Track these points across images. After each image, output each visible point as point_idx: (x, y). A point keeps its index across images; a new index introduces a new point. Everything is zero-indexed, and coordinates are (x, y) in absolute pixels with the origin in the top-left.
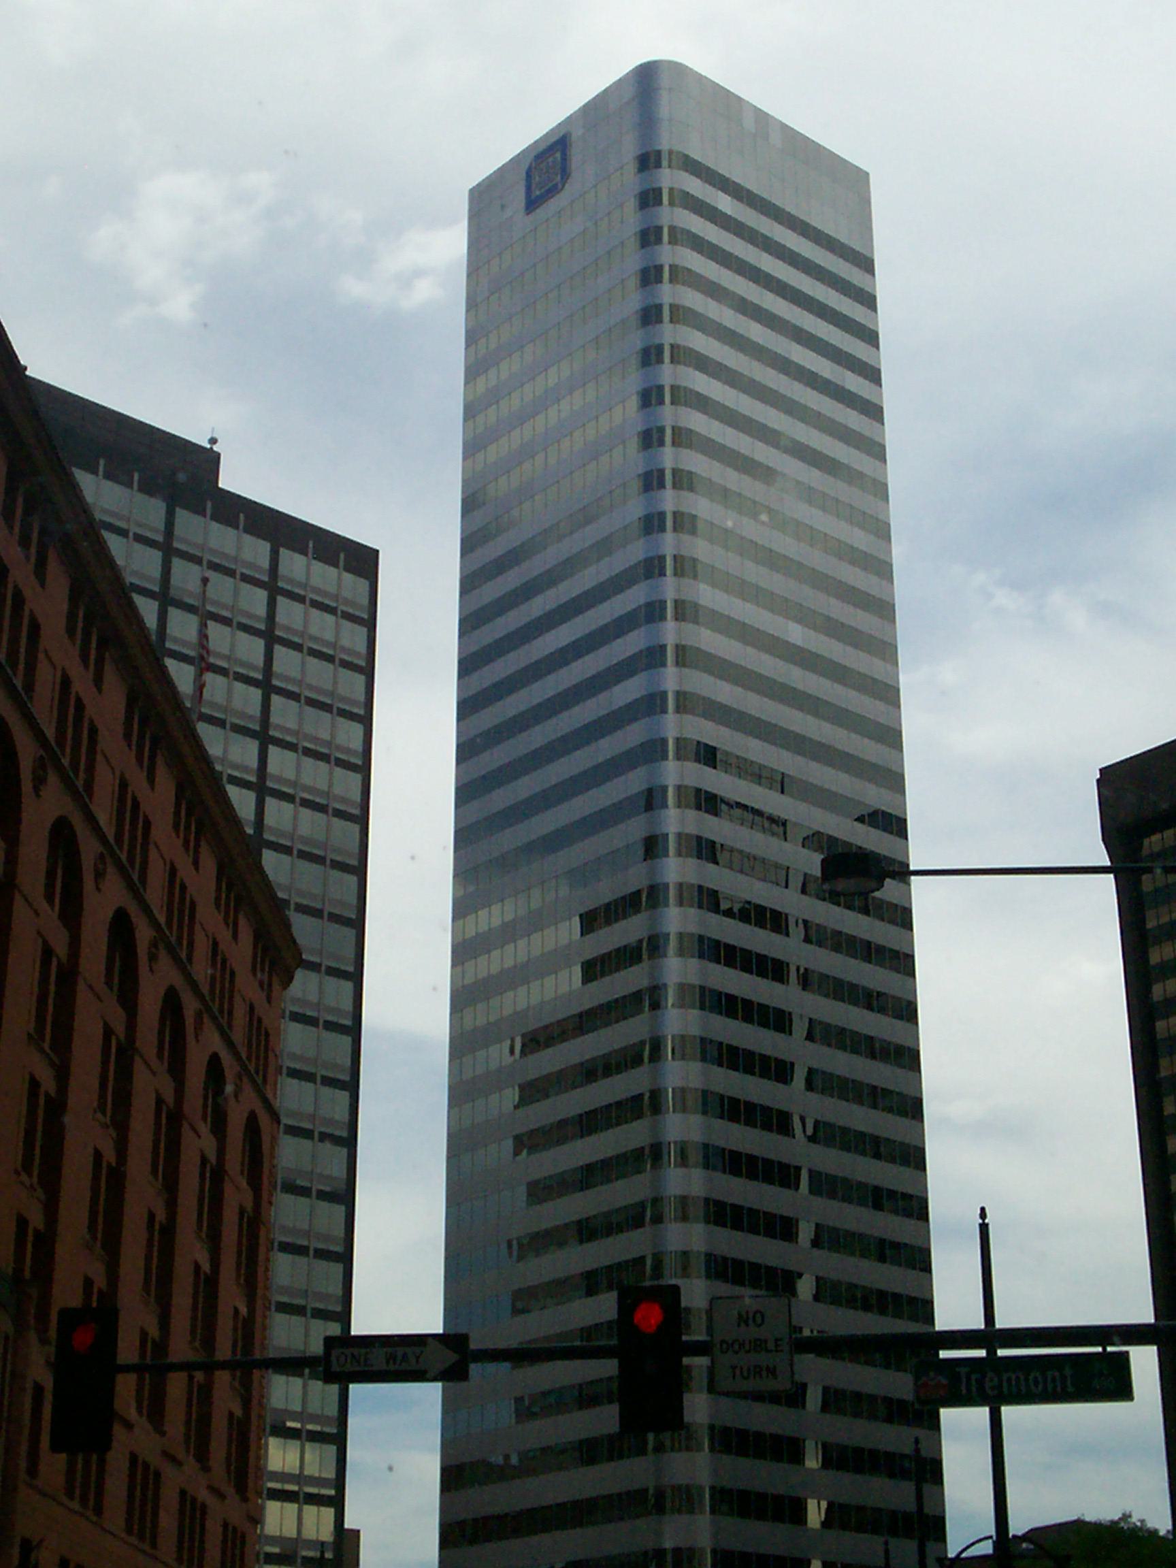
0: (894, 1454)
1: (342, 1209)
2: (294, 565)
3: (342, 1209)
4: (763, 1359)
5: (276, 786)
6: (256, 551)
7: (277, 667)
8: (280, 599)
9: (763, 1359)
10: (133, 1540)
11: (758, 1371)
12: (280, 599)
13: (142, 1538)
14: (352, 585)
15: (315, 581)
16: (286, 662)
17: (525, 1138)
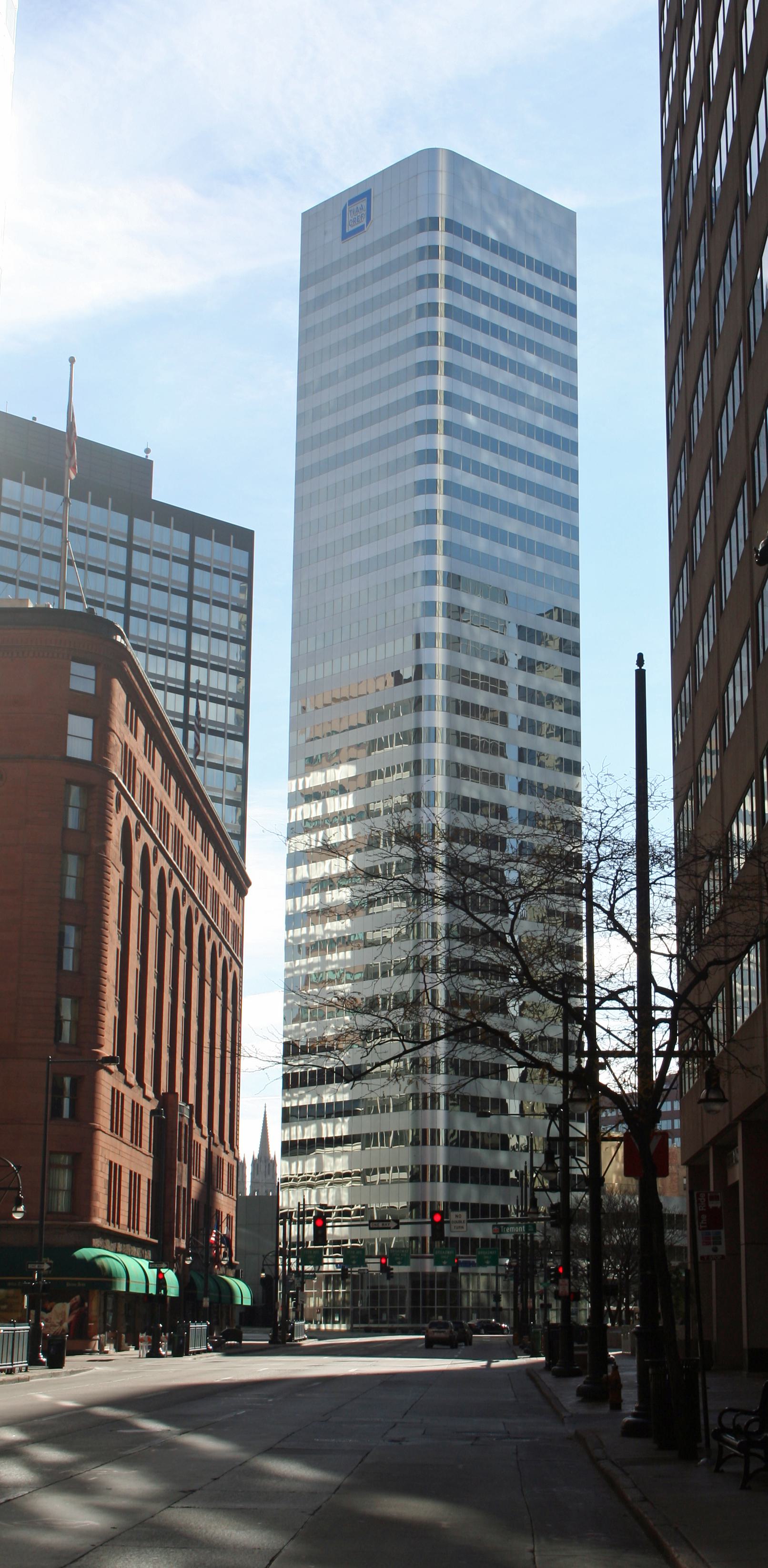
0: (469, 579)
1: (246, 554)
2: (205, 548)
3: (246, 554)
4: (461, 1225)
5: (200, 562)
6: (180, 540)
7: (197, 551)
8: (194, 602)
9: (461, 1225)
10: (114, 1134)
11: (460, 1227)
12: (194, 602)
13: (117, 1133)
14: (239, 557)
15: (215, 620)
16: (201, 579)
17: (335, 880)
